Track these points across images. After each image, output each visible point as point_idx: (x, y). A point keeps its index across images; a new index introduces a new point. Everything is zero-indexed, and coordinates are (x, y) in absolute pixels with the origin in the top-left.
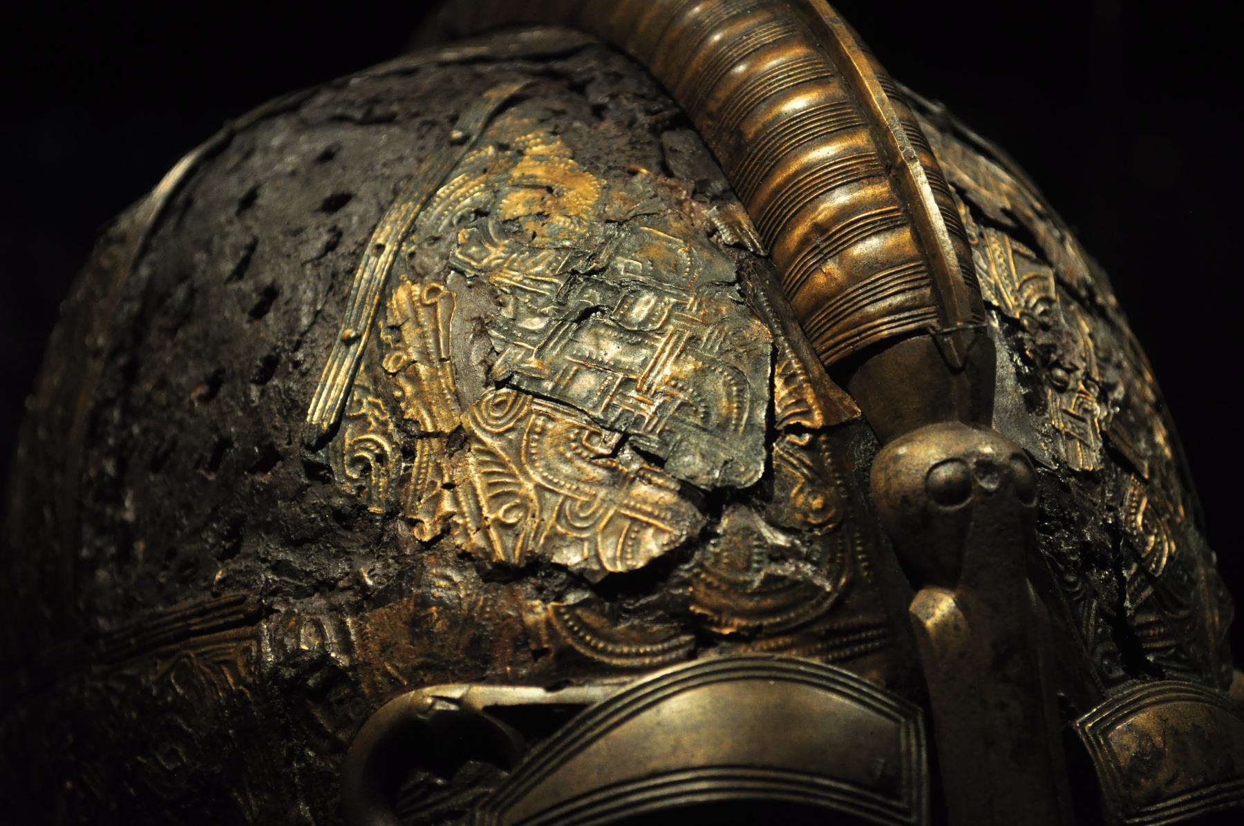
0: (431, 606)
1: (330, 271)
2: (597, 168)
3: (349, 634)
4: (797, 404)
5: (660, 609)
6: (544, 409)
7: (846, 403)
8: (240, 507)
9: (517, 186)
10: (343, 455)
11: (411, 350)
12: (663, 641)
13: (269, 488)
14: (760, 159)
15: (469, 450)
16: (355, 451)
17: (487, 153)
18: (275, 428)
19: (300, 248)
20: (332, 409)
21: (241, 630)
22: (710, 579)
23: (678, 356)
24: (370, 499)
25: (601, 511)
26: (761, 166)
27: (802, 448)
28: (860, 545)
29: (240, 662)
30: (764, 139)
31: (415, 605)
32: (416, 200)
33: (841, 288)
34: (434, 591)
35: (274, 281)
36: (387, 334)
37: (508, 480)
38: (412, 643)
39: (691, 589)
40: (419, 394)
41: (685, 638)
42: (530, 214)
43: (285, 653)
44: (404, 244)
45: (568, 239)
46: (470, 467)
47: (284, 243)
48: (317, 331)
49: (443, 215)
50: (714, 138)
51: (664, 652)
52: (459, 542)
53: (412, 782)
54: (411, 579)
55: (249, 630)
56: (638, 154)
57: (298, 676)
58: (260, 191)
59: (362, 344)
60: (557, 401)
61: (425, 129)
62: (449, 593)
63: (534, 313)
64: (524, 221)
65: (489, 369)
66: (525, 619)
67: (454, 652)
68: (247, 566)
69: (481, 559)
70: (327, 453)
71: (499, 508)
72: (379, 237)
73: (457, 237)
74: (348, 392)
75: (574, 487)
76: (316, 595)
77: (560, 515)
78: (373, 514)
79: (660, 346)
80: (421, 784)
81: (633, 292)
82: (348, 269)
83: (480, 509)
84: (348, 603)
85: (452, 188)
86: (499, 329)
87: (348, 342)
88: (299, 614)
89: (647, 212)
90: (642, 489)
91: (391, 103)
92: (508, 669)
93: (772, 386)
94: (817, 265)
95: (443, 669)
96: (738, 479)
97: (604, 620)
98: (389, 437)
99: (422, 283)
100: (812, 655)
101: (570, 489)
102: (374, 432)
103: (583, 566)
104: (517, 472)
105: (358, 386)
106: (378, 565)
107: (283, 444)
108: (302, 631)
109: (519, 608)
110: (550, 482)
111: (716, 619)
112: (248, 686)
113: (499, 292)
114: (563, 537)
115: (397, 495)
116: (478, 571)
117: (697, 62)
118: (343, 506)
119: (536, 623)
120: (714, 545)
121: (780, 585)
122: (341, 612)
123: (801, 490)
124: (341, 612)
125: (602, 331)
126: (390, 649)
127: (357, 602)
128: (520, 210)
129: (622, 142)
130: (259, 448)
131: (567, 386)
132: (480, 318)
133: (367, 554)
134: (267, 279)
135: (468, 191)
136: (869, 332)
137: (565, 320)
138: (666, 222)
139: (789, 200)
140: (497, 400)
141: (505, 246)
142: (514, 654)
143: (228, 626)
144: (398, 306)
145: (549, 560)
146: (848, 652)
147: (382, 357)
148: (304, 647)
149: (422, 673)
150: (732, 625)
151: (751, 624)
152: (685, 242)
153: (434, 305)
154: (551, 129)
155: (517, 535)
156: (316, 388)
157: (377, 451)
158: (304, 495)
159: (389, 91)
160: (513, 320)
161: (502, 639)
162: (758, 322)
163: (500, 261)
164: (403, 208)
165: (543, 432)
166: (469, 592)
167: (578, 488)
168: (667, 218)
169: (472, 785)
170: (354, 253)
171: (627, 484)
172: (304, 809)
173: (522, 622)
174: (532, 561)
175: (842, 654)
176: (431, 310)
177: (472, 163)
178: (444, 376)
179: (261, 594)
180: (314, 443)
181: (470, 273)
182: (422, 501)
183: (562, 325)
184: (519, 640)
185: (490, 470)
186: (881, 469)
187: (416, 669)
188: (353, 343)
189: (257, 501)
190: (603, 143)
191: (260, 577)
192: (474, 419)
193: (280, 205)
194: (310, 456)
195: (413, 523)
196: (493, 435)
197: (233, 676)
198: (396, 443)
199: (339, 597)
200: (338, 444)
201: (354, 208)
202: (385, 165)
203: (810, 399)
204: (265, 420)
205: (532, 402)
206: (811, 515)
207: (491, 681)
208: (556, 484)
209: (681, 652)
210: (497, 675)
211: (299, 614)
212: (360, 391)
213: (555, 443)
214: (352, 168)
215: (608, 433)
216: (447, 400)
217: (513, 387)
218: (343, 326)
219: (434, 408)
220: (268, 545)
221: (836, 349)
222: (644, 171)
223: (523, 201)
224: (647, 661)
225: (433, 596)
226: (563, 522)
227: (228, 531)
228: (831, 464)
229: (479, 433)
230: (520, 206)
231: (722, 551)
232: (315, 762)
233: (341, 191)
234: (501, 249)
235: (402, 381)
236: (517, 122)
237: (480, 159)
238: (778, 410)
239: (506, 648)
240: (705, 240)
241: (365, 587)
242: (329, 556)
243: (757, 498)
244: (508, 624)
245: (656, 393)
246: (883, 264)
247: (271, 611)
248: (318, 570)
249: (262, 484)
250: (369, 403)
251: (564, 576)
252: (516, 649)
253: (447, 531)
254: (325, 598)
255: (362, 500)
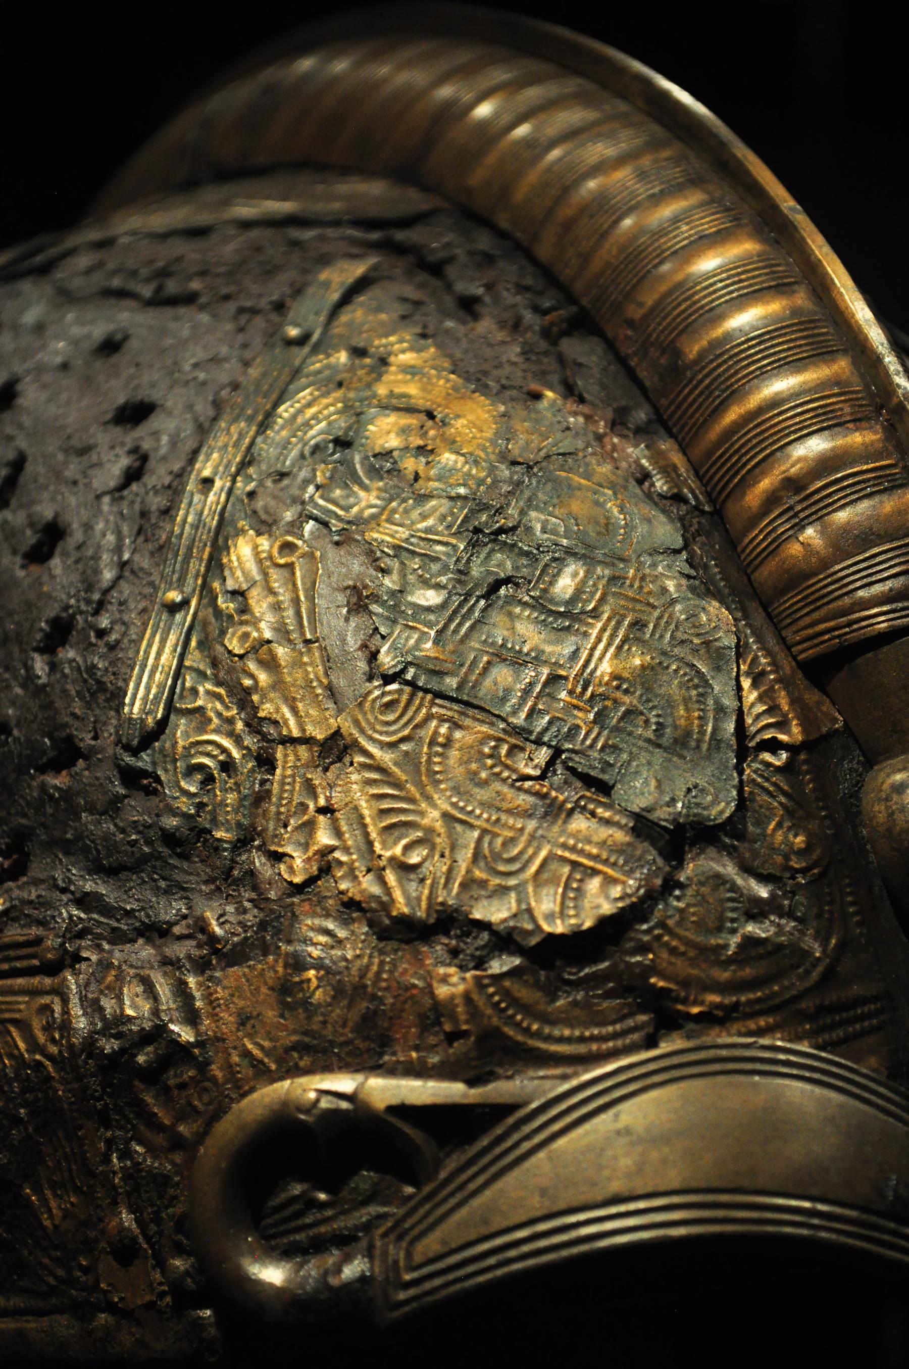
0: (308, 969)
1: (137, 507)
2: (486, 386)
3: (193, 998)
4: (769, 712)
5: (610, 981)
6: (449, 713)
7: (824, 709)
8: (25, 815)
9: (386, 408)
10: (175, 761)
11: (263, 625)
12: (613, 1022)
13: (67, 795)
14: (707, 387)
15: (352, 764)
16: (192, 756)
17: (338, 359)
18: (74, 715)
19: (91, 472)
20: (157, 697)
21: (35, 981)
22: (674, 943)
23: (619, 648)
24: (214, 821)
25: (530, 851)
26: (707, 398)
27: (778, 769)
28: (850, 894)
29: (37, 1025)
30: (711, 361)
31: (286, 966)
32: (250, 420)
33: (825, 564)
34: (310, 949)
35: (57, 515)
36: (225, 602)
37: (405, 806)
38: (282, 1016)
39: (651, 956)
40: (278, 685)
41: (642, 1018)
42: (407, 448)
43: (103, 1019)
44: (239, 478)
45: (464, 485)
46: (354, 786)
47: (66, 463)
48: (126, 589)
49: (289, 443)
50: (635, 353)
51: (615, 1036)
52: (343, 886)
53: (282, 1197)
54: (278, 932)
55: (48, 981)
56: (535, 368)
57: (123, 1051)
58: (19, 387)
59: (192, 611)
60: (467, 704)
61: (243, 319)
62: (333, 952)
63: (426, 584)
64: (401, 457)
65: (373, 656)
66: (437, 992)
67: (340, 1030)
68: (39, 897)
69: (374, 911)
70: (153, 755)
71: (396, 843)
72: (204, 468)
73: (315, 476)
74: (177, 675)
75: (494, 818)
76: (141, 941)
77: (477, 856)
78: (220, 840)
79: (594, 632)
80: (294, 1199)
81: (555, 559)
82: (162, 508)
83: (370, 844)
84: (189, 957)
85: (297, 405)
86: (383, 604)
87: (173, 608)
88: (120, 967)
89: (561, 451)
90: (579, 823)
91: (190, 278)
92: (414, 1055)
93: (739, 688)
94: (790, 533)
95: (325, 1051)
96: (705, 813)
97: (539, 994)
98: (238, 740)
99: (270, 536)
100: (798, 1039)
101: (488, 820)
102: (216, 731)
103: (511, 924)
104: (418, 796)
105: (190, 668)
106: (230, 909)
107: (86, 740)
108: (125, 990)
109: (428, 977)
110: (462, 809)
111: (683, 994)
112: (50, 1057)
113: (378, 554)
114: (483, 884)
115: (253, 816)
116: (370, 925)
117: (608, 251)
118: (177, 828)
119: (452, 997)
120: (678, 899)
121: (761, 950)
122: (179, 968)
123: (779, 825)
124: (179, 968)
125: (518, 610)
126: (252, 1022)
127: (202, 957)
128: (393, 442)
129: (514, 352)
130: (50, 739)
131: (477, 683)
132: (355, 587)
133: (212, 892)
134: (47, 511)
135: (320, 412)
136: (864, 623)
137: (468, 595)
138: (587, 465)
139: (750, 445)
140: (387, 699)
141: (379, 489)
142: (421, 1036)
143: (15, 973)
144: (240, 563)
145: (467, 916)
146: (841, 1033)
147: (223, 633)
148: (130, 1012)
149: (295, 1055)
150: (702, 1003)
151: (727, 1001)
152: (615, 494)
153: (290, 566)
154: (418, 330)
155: (422, 880)
156: (133, 669)
157: (221, 758)
158: (118, 809)
159: (179, 259)
160: (401, 591)
161: (404, 1015)
162: (716, 604)
163: (373, 510)
164: (233, 429)
165: (448, 743)
166: (358, 952)
167: (498, 820)
168: (588, 459)
169: (365, 1203)
170: (169, 487)
171: (563, 816)
172: (127, 1218)
173: (432, 994)
174: (444, 916)
175: (834, 1036)
176: (285, 573)
177: (319, 372)
178: (311, 664)
179: (64, 936)
180: (135, 742)
181: (335, 525)
182: (289, 829)
183: (466, 600)
184: (428, 1017)
185: (381, 791)
186: (880, 800)
187: (288, 1050)
188: (180, 610)
189: (50, 810)
190: (488, 352)
191: (61, 914)
192: (357, 723)
193: (52, 409)
194: (128, 759)
195: (277, 857)
196: (384, 745)
197: (25, 1040)
198: (247, 748)
199: (176, 947)
200: (168, 745)
201: (155, 422)
202: (196, 366)
203: (784, 704)
204: (59, 704)
205: (432, 704)
206: (793, 857)
207: (391, 1071)
208: (462, 809)
209: (636, 1036)
210: (398, 1062)
211: (120, 967)
212: (193, 675)
213: (465, 758)
214: (151, 366)
215: (534, 746)
216: (317, 695)
217: (407, 683)
218: (163, 586)
219: (300, 705)
220: (69, 870)
221: (815, 641)
222: (549, 394)
223: (395, 429)
224: (594, 1047)
225: (310, 956)
226: (482, 864)
227: (6, 844)
228: (814, 790)
229: (363, 742)
230: (392, 435)
231: (689, 905)
232: (145, 1160)
233: (139, 398)
234: (374, 493)
235: (252, 666)
236: (371, 318)
237: (328, 367)
238: (749, 720)
239: (409, 1027)
240: (638, 491)
241: (213, 939)
242: (157, 890)
243: (726, 835)
244: (413, 996)
245: (593, 695)
246: (879, 536)
247: (77, 958)
248: (143, 909)
249: (56, 788)
250: (208, 692)
251: (485, 936)
252: (424, 1029)
253: (326, 869)
254: (155, 947)
255: (204, 821)
